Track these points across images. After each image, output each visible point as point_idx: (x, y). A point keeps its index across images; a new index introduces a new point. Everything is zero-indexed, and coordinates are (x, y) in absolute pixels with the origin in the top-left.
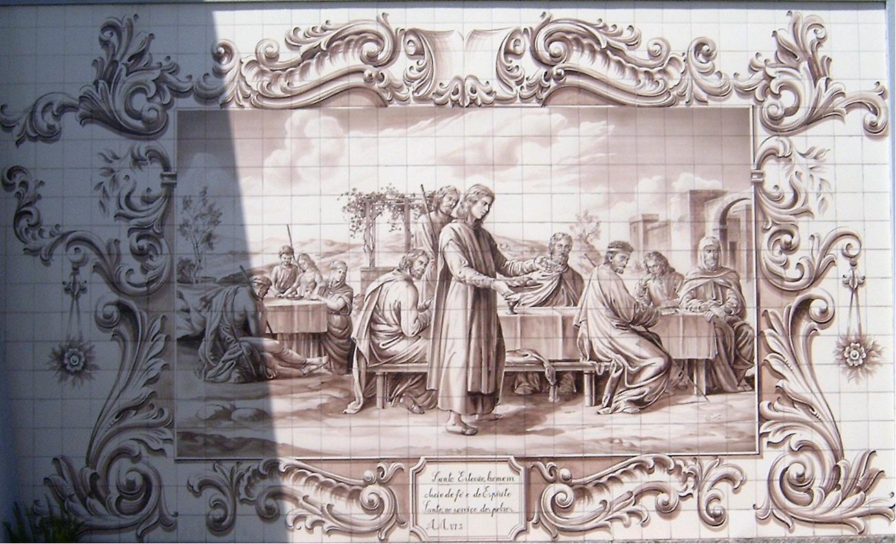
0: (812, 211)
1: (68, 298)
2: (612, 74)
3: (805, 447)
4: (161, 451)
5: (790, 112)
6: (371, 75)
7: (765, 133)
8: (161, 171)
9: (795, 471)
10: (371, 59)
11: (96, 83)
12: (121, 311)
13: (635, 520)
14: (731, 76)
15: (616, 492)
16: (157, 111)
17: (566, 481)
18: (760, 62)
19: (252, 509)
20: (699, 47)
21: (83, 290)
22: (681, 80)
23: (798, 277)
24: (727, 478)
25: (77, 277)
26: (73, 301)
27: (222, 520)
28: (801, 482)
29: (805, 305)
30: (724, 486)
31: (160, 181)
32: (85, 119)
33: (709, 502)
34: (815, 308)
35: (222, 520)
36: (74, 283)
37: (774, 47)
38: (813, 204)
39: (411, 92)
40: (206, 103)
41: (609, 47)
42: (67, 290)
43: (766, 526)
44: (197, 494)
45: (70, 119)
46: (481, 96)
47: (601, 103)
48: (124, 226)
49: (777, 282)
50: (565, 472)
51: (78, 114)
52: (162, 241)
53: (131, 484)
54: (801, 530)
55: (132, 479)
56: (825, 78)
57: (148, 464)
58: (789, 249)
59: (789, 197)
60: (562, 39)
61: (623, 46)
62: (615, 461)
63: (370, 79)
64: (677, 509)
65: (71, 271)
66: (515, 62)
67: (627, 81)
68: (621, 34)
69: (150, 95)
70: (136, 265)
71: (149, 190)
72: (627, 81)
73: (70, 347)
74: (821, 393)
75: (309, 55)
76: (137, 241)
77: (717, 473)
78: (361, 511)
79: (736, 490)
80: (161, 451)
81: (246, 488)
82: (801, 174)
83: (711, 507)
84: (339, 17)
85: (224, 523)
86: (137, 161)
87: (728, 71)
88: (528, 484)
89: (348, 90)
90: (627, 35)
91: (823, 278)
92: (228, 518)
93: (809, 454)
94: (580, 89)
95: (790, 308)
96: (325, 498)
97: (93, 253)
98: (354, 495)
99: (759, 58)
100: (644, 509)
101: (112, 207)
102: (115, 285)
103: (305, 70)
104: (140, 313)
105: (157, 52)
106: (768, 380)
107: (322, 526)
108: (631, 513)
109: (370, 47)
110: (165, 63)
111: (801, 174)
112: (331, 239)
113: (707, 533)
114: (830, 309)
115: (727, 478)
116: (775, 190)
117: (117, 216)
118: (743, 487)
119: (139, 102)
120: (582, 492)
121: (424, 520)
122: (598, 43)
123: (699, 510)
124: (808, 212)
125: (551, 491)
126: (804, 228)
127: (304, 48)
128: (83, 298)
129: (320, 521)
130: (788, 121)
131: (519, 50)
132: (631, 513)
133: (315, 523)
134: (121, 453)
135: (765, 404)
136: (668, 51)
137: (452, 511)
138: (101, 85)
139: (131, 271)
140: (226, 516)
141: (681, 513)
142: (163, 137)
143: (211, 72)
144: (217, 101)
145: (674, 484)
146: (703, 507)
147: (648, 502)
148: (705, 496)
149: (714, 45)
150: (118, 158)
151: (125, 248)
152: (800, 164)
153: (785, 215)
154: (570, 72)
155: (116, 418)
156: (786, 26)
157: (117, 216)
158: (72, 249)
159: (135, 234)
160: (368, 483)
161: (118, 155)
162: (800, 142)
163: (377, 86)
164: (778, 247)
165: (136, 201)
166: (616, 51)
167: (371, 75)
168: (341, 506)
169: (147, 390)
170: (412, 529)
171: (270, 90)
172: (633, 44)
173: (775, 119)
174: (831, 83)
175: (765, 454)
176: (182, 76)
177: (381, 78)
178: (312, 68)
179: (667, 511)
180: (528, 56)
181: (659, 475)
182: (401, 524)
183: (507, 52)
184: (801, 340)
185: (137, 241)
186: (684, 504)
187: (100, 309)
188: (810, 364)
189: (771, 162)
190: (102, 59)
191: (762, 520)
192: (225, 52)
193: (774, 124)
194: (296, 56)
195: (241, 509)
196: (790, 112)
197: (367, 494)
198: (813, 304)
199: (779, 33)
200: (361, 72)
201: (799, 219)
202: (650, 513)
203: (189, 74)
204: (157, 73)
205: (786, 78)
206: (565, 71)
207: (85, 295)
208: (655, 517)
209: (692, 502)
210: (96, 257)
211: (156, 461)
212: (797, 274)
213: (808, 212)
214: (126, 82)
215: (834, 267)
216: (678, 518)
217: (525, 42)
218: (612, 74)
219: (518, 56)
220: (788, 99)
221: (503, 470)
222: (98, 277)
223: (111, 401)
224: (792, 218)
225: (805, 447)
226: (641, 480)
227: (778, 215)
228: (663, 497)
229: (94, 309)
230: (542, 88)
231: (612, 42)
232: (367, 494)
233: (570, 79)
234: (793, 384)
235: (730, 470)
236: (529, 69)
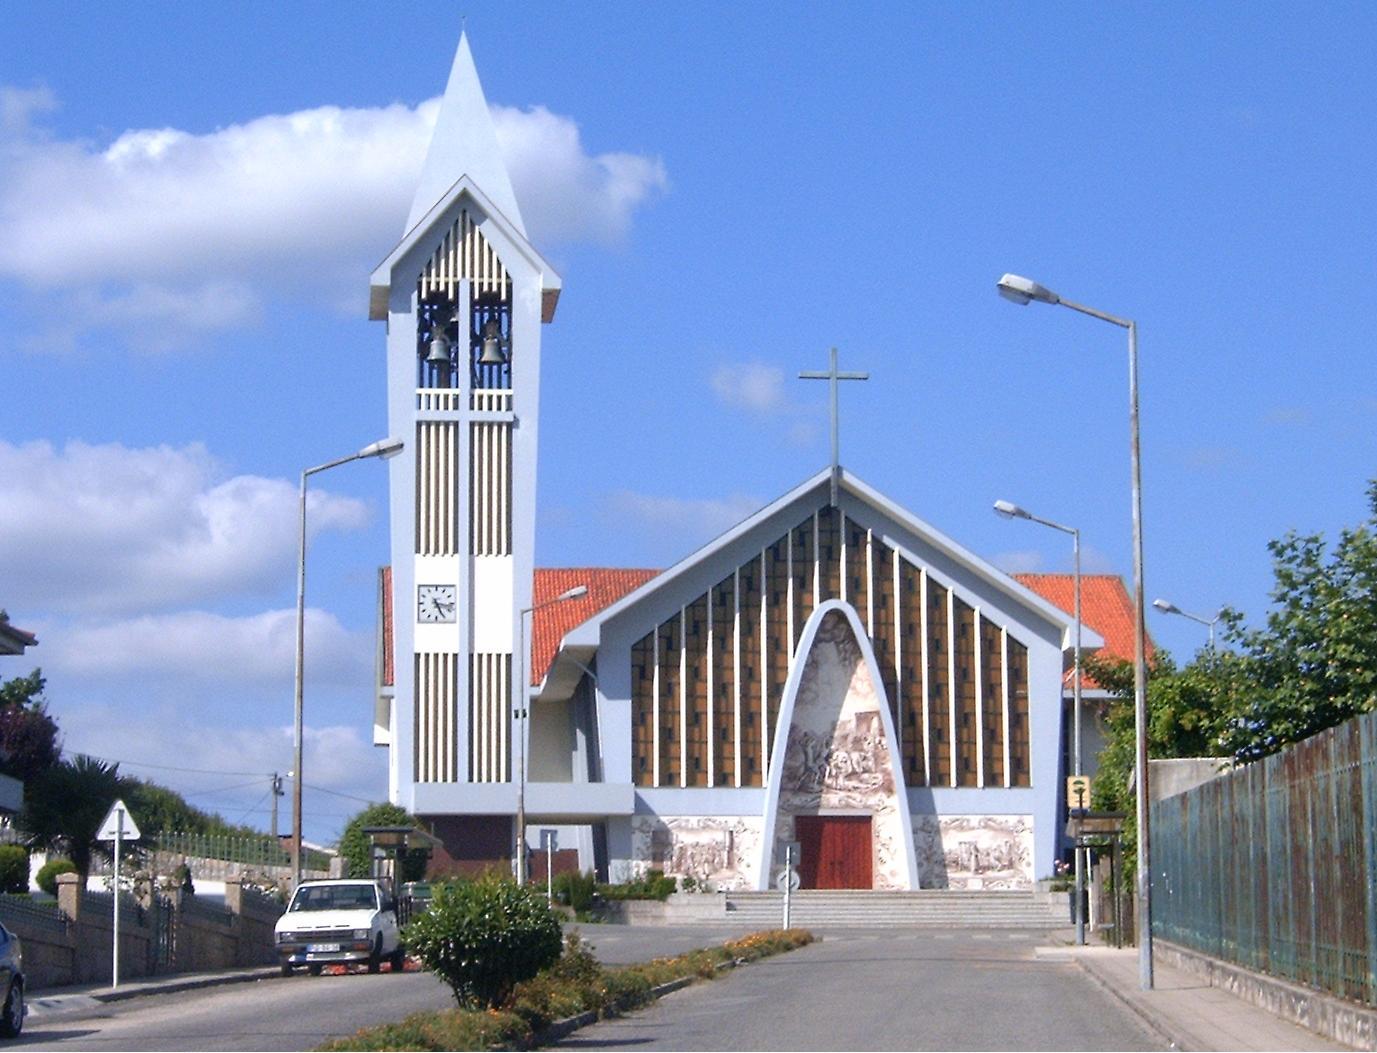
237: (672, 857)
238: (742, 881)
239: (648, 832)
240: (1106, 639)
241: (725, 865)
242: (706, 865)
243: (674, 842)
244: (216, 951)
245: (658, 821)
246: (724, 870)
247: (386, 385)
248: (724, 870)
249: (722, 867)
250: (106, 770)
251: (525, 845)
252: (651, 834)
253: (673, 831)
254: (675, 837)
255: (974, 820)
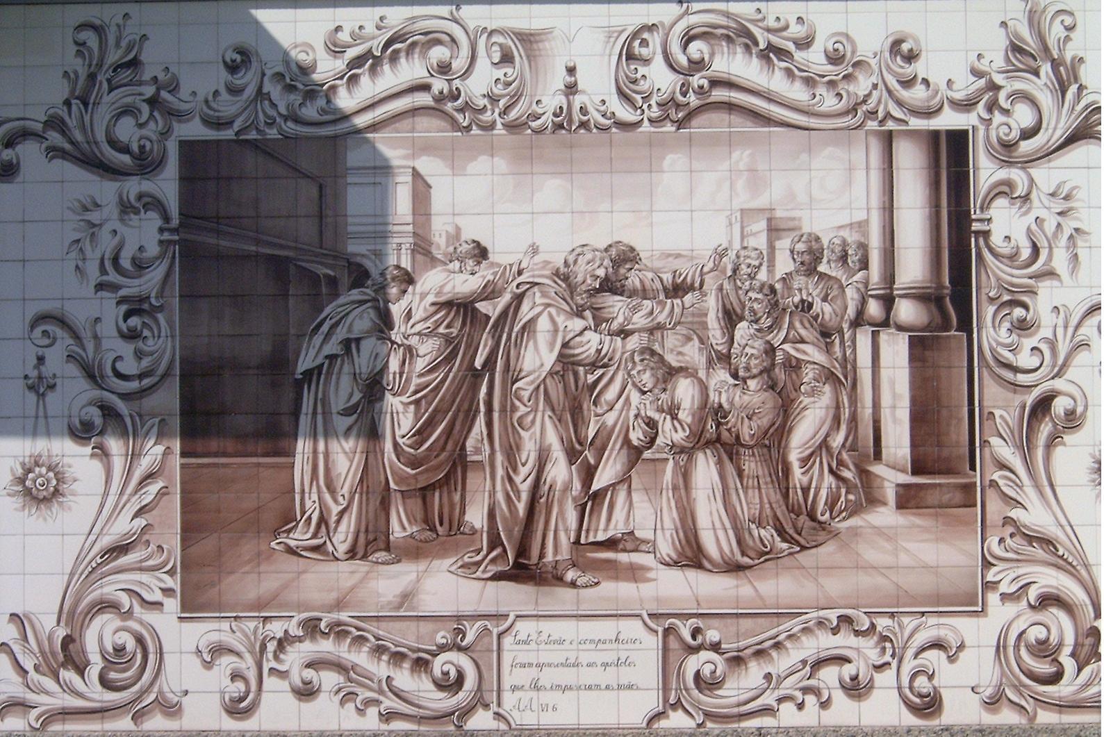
0: (1058, 272)
1: (32, 397)
2: (777, 82)
3: (1049, 600)
4: (157, 605)
5: (1028, 134)
6: (441, 93)
7: (992, 165)
8: (159, 222)
9: (1037, 633)
10: (444, 68)
11: (67, 103)
12: (104, 415)
13: (811, 700)
14: (943, 86)
15: (781, 663)
16: (151, 141)
17: (715, 647)
18: (983, 66)
19: (285, 685)
20: (897, 44)
21: (52, 387)
22: (871, 92)
23: (1038, 365)
24: (938, 645)
25: (43, 368)
26: (38, 402)
27: (242, 699)
28: (1044, 649)
29: (1043, 405)
30: (933, 655)
31: (158, 237)
32: (55, 152)
33: (913, 677)
34: (1060, 406)
35: (242, 699)
36: (40, 378)
37: (1003, 43)
38: (1060, 262)
39: (496, 114)
40: (218, 129)
41: (771, 47)
42: (31, 388)
43: (830, 710)
44: (208, 665)
45: (30, 153)
46: (595, 116)
47: (754, 125)
48: (109, 299)
49: (1009, 375)
50: (712, 635)
51: (44, 146)
52: (160, 316)
53: (120, 650)
54: (1046, 717)
55: (120, 642)
56: (1077, 86)
57: (141, 622)
58: (1023, 327)
59: (1026, 253)
60: (703, 36)
61: (791, 47)
62: (782, 620)
63: (441, 98)
64: (870, 686)
65: (35, 361)
66: (642, 70)
67: (798, 93)
68: (786, 27)
69: (142, 120)
70: (127, 349)
71: (141, 249)
72: (798, 93)
73: (37, 464)
74: (1071, 526)
75: (358, 62)
76: (125, 321)
77: (921, 638)
78: (432, 687)
79: (952, 659)
80: (157, 605)
81: (275, 652)
82: (1043, 220)
83: (916, 684)
84: (397, 16)
85: (243, 705)
86: (126, 208)
87: (938, 79)
88: (666, 649)
89: (415, 111)
90: (796, 30)
91: (1069, 366)
92: (251, 696)
93: (1054, 610)
94: (730, 107)
95: (1024, 407)
96: (381, 669)
97: (66, 335)
98: (421, 665)
99: (982, 61)
100: (822, 685)
101: (92, 269)
102: (92, 374)
103: (354, 80)
104: (131, 416)
105: (154, 60)
106: (995, 508)
107: (379, 706)
108: (806, 690)
109: (439, 53)
110: (161, 76)
111: (1043, 220)
112: (632, 244)
113: (229, 724)
114: (1080, 410)
115: (938, 645)
116: (1006, 244)
117: (100, 287)
118: (961, 655)
119: (126, 130)
120: (737, 661)
121: (509, 699)
122: (756, 43)
123: (899, 688)
124: (1051, 274)
125: (693, 664)
126: (1046, 299)
127: (352, 53)
128: (51, 397)
129: (377, 701)
130: (1026, 146)
131: (644, 52)
132: (806, 690)
133: (369, 702)
134: (107, 606)
135: (993, 542)
136: (854, 52)
137: (603, 687)
138: (74, 108)
139: (119, 358)
140: (247, 693)
141: (875, 692)
142: (162, 176)
143: (223, 90)
144: (232, 127)
145: (869, 650)
146: (905, 681)
147: (829, 675)
148: (909, 666)
149: (917, 41)
150: (98, 206)
151: (108, 329)
152: (1041, 207)
153: (1019, 277)
154: (715, 83)
155: (101, 558)
156: (1020, 16)
157: (100, 287)
158: (38, 331)
159: (124, 308)
160: (443, 648)
161: (99, 203)
162: (1046, 176)
163: (449, 107)
164: (1006, 325)
165: (126, 263)
166: (782, 53)
167: (441, 93)
168: (404, 679)
169: (141, 522)
170: (496, 709)
171: (300, 110)
172: (805, 43)
173: (1008, 146)
174: (1085, 92)
175: (990, 610)
176: (184, 93)
177: (455, 96)
178: (365, 80)
179: (856, 689)
180: (659, 60)
181: (844, 642)
182: (486, 706)
183: (631, 57)
184: (1040, 453)
185: (125, 321)
186: (879, 678)
187: (75, 411)
188: (1052, 486)
189: (1001, 202)
190: (76, 73)
191: (993, 703)
192: (242, 61)
193: (1006, 150)
194: (340, 64)
195: (270, 682)
196: (1028, 134)
197: (439, 664)
198: (1056, 401)
199: (1010, 23)
200: (425, 88)
201: (1039, 284)
202: (832, 691)
203: (190, 92)
204: (149, 91)
205: (1018, 85)
206: (710, 81)
207: (53, 394)
208: (839, 697)
209: (890, 674)
210: (71, 341)
211: (151, 617)
212: (1034, 362)
213: (1051, 274)
214: (108, 102)
215: (1087, 352)
216: (869, 700)
217: (655, 40)
218: (777, 82)
219: (646, 62)
220: (1023, 116)
221: (633, 629)
222: (73, 370)
223: (92, 538)
224: (1031, 282)
225: (1049, 600)
226: (825, 642)
227: (1009, 278)
228: (848, 670)
229: (66, 413)
230: (678, 106)
231: (775, 40)
232: (439, 664)
233: (719, 94)
234: (1036, 516)
235: (942, 633)
236: (660, 78)
237: (374, 388)
238: (1062, 627)
239: (147, 164)
240: (719, 631)
241: (890, 478)
242: (705, 470)
243: (399, 256)
244: (296, 596)
245: (242, 59)
246: (886, 516)
247: (509, 3)
248: (886, 516)
249: (870, 497)
250: (306, 386)
251: (850, 470)
252: (167, 185)
253: (390, 147)
254: (402, 203)
255: (851, 497)
